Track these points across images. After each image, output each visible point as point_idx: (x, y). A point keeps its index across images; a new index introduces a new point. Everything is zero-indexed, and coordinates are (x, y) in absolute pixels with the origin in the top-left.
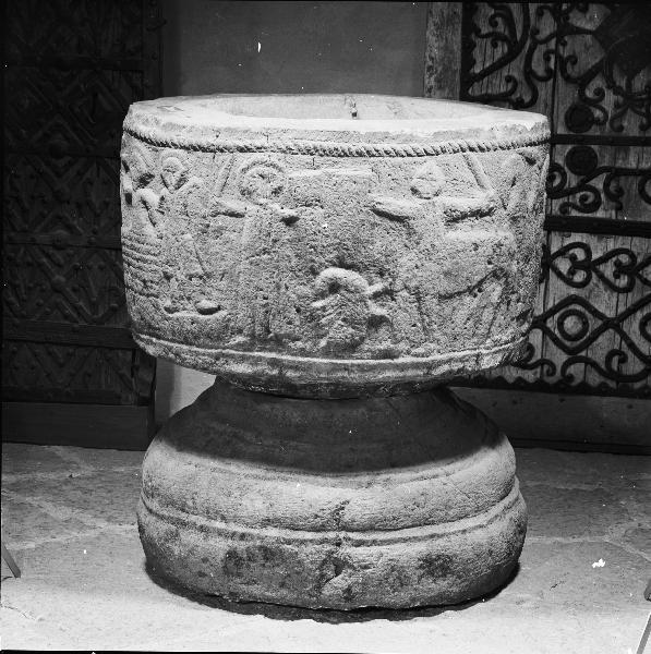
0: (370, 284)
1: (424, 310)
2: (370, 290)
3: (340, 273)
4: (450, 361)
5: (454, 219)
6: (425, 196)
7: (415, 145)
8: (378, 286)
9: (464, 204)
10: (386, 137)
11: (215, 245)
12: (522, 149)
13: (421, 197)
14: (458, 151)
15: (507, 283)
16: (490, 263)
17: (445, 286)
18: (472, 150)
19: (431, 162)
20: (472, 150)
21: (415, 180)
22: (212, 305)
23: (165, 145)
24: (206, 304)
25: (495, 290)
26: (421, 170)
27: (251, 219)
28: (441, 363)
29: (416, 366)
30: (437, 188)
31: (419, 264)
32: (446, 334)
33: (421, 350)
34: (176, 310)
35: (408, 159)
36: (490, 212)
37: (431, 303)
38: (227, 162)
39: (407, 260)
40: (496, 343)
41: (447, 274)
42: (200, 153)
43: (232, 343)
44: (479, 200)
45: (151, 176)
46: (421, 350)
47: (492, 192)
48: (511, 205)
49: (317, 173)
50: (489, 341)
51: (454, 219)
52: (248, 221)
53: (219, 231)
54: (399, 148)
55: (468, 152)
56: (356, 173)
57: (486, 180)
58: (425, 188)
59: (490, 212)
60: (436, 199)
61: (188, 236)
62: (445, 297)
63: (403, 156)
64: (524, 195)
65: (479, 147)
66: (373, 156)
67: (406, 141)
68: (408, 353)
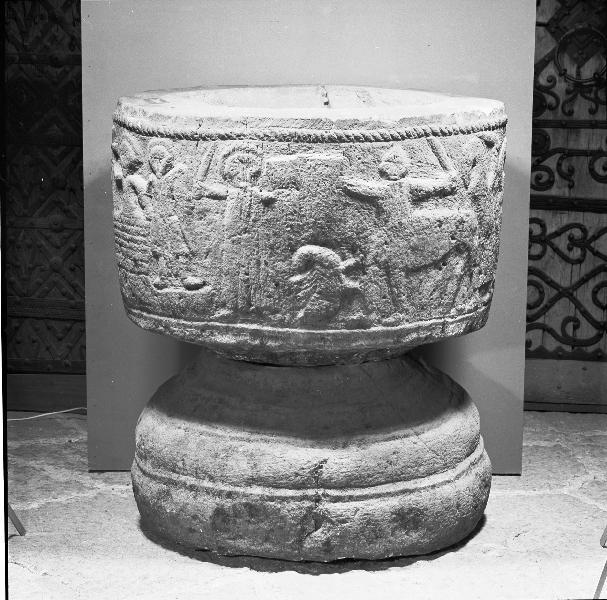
0: (344, 259)
1: (393, 283)
2: (343, 265)
3: (315, 249)
4: (417, 329)
5: (419, 198)
6: (392, 177)
7: (383, 131)
8: (351, 261)
9: (428, 184)
10: (355, 124)
11: (199, 226)
12: (481, 133)
13: (389, 179)
14: (422, 136)
15: (469, 257)
16: (453, 238)
17: (411, 260)
18: (435, 134)
19: (398, 148)
20: (435, 134)
21: (383, 163)
22: (197, 281)
23: (152, 134)
24: (192, 280)
25: (458, 264)
26: (386, 155)
27: (233, 201)
28: (409, 331)
29: (386, 334)
30: (403, 171)
31: (388, 240)
32: (413, 304)
33: (391, 319)
34: (165, 286)
35: (375, 144)
36: (453, 191)
37: (400, 276)
38: (209, 150)
39: (376, 237)
40: (460, 312)
41: (414, 249)
42: (184, 141)
43: (217, 315)
44: (442, 180)
45: (140, 163)
46: (391, 319)
47: (454, 173)
48: (472, 184)
49: (293, 157)
50: (453, 311)
51: (419, 198)
52: (230, 203)
53: (203, 213)
54: (368, 133)
55: (432, 137)
56: (328, 158)
57: (448, 162)
58: (392, 169)
59: (453, 191)
60: (402, 180)
61: (175, 218)
62: (411, 271)
63: (371, 141)
64: (484, 175)
65: (441, 131)
66: (344, 141)
67: (374, 128)
68: (379, 322)
